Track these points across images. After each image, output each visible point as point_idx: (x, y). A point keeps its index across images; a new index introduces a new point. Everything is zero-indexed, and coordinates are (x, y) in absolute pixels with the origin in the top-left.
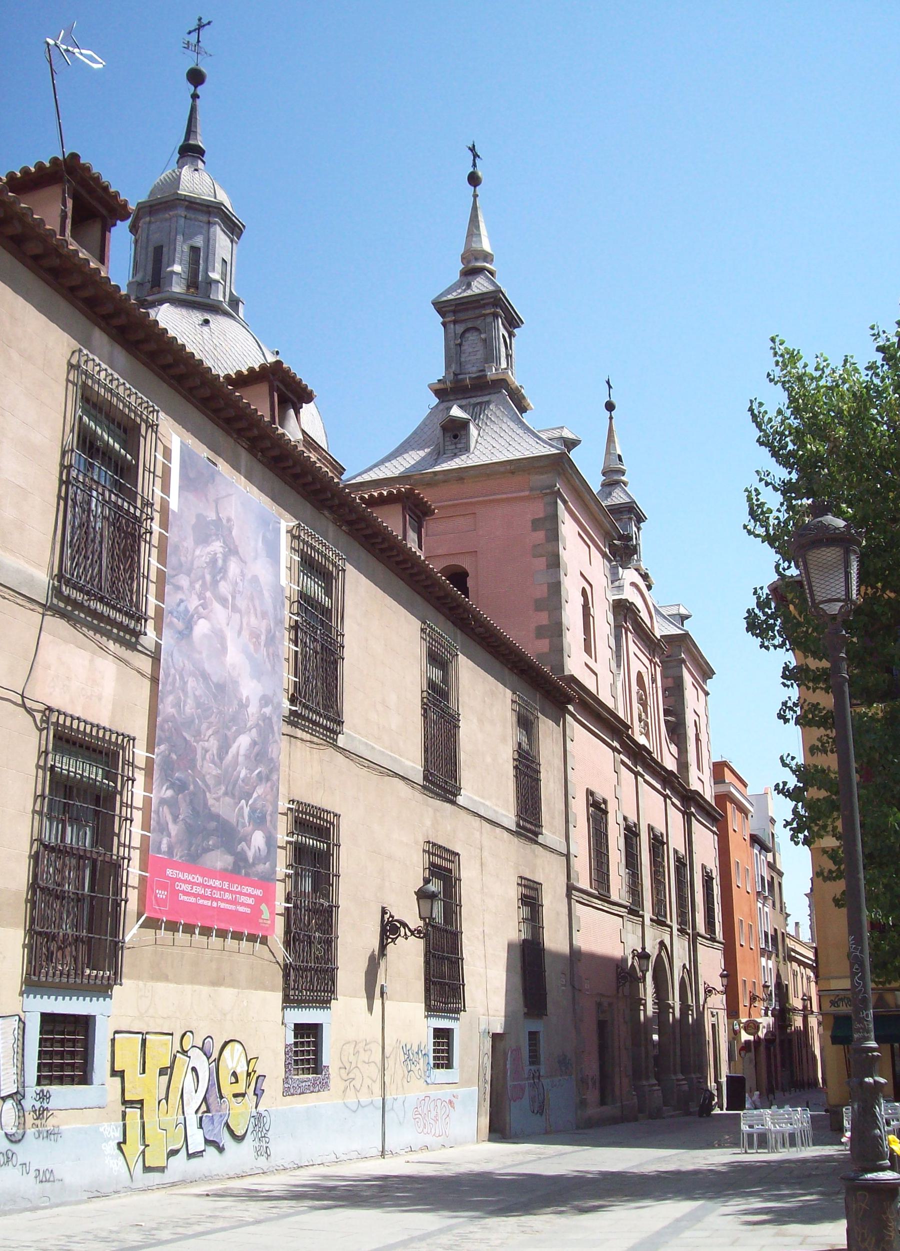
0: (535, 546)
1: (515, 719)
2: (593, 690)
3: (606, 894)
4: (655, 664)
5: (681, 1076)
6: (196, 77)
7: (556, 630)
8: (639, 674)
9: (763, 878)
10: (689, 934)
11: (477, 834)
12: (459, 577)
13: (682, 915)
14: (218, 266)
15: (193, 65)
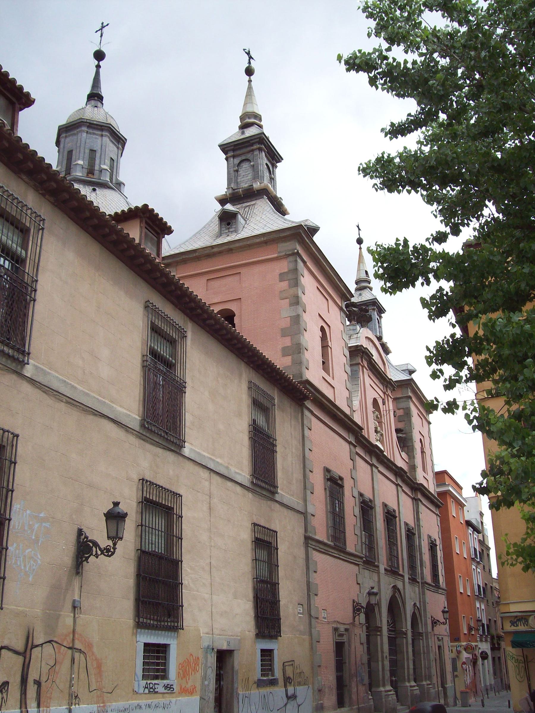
0: (281, 292)
1: (250, 401)
2: (331, 397)
4: (388, 395)
5: (413, 683)
6: (99, 56)
7: (297, 350)
8: (375, 400)
9: (475, 549)
10: (418, 582)
11: (207, 483)
12: (229, 316)
13: (412, 567)
14: (108, 162)
15: (97, 48)
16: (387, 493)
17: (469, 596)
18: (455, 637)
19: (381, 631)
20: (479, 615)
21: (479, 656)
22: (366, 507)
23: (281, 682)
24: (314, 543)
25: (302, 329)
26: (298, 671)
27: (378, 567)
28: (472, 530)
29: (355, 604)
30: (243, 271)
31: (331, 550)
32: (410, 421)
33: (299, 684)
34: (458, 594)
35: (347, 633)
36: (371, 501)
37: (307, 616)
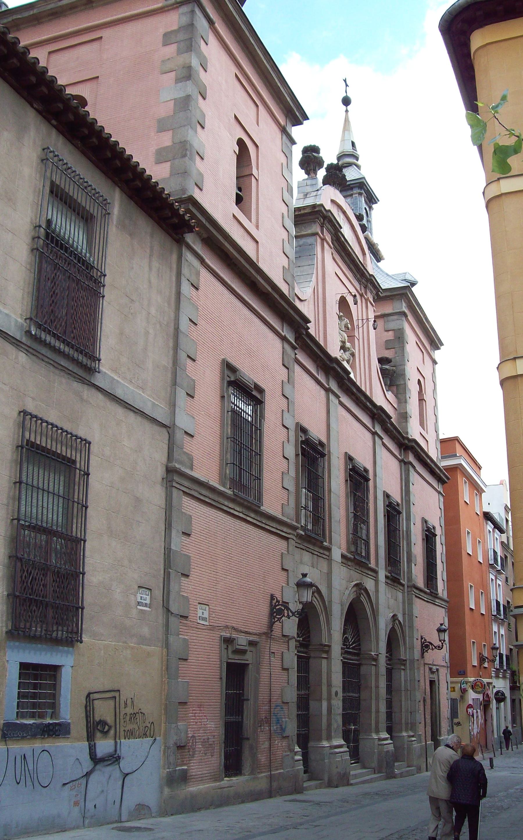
0: (163, 61)
3: (256, 502)
9: (495, 553)
10: (403, 585)
16: (351, 438)
17: (482, 614)
18: (458, 668)
19: (328, 652)
20: (496, 641)
21: (492, 696)
22: (311, 454)
23: (79, 728)
24: (186, 483)
25: (194, 121)
26: (129, 710)
27: (329, 550)
28: (493, 526)
29: (423, 640)
30: (105, 33)
31: (226, 503)
32: (402, 348)
33: (130, 734)
34: (467, 611)
35: (252, 649)
36: (321, 444)
37: (161, 610)
